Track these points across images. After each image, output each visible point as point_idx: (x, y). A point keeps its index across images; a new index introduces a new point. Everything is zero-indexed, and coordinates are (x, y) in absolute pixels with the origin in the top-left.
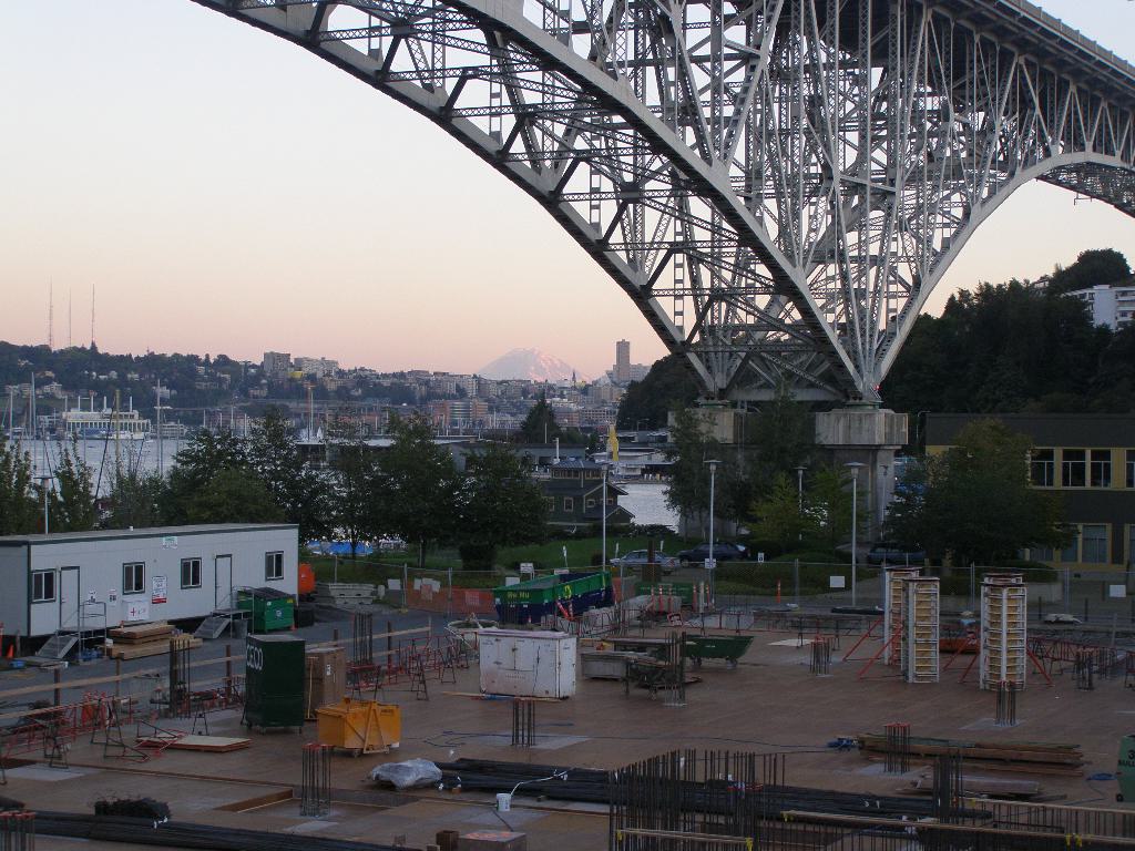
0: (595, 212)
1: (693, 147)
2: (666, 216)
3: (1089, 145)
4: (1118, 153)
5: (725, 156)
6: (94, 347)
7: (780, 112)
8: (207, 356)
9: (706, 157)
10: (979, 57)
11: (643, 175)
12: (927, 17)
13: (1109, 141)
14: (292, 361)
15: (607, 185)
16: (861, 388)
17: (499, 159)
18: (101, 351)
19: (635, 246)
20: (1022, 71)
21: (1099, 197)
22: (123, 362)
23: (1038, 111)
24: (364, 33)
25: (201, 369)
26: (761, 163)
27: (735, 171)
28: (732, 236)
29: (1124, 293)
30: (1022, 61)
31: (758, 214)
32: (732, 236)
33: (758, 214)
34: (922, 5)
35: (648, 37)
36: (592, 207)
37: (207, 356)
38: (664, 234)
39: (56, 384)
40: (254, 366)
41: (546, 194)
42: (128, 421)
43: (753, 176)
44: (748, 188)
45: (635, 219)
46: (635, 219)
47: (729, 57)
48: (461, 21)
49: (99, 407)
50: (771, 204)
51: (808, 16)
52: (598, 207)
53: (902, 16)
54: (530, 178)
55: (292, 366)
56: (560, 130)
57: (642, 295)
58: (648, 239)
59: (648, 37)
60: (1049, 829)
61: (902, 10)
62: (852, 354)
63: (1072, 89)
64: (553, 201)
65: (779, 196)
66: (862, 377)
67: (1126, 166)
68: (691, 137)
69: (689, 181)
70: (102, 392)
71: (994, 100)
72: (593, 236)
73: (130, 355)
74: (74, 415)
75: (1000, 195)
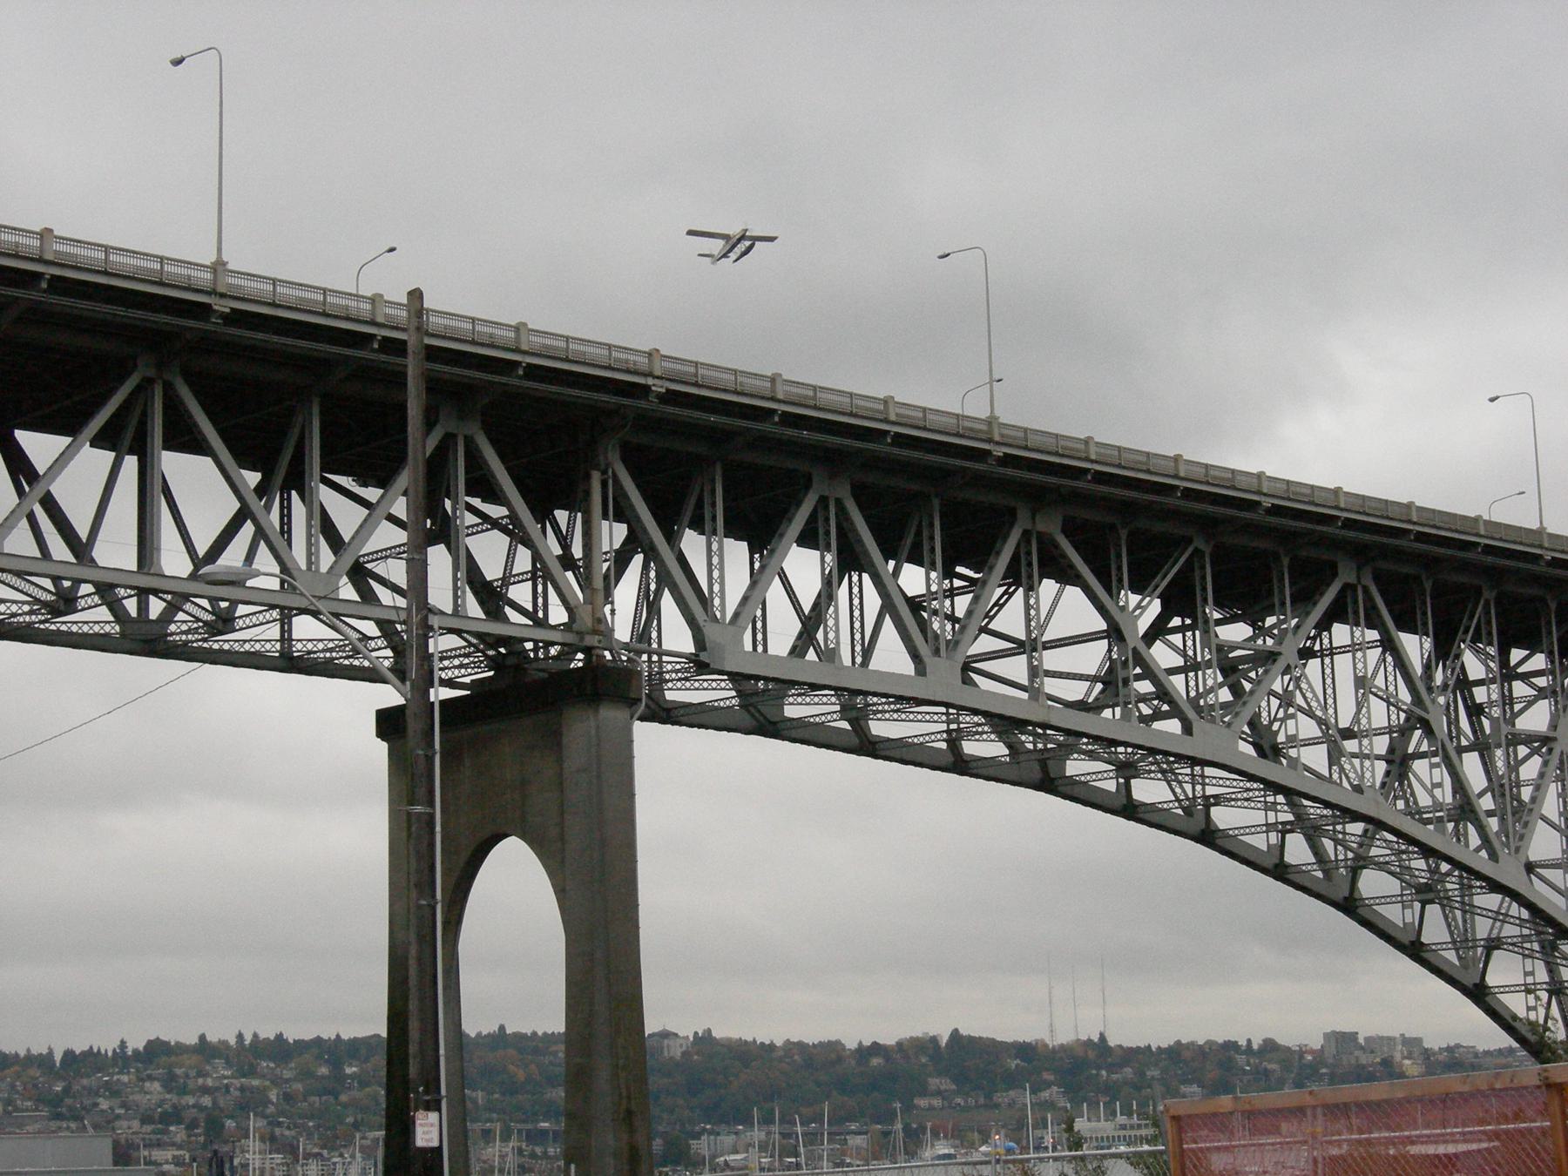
1: (1478, 850)
6: (1102, 1037)
8: (1249, 1041)
9: (1493, 856)
14: (1361, 1041)
17: (1280, 871)
18: (1112, 1043)
24: (1111, 774)
25: (1241, 1059)
37: (1249, 1041)
39: (1055, 1088)
40: (1312, 1052)
41: (1341, 902)
55: (1362, 1048)
57: (1479, 994)
60: (154, 1142)
68: (1474, 840)
73: (1149, 1046)
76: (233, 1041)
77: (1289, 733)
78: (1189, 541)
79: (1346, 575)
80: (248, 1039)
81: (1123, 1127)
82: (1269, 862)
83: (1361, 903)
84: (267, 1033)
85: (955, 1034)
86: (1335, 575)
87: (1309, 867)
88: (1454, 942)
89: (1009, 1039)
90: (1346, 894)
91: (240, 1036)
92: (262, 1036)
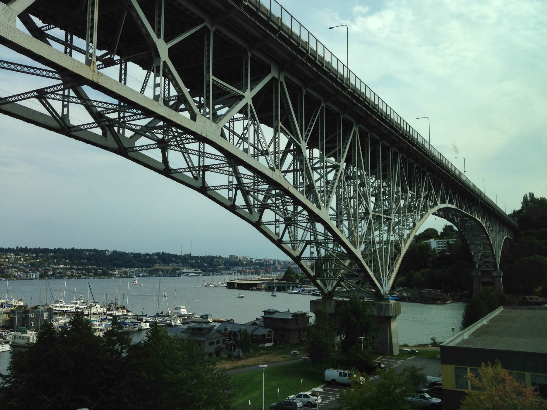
0: (277, 229)
2: (306, 231)
3: (447, 201)
4: (455, 204)
5: (327, 206)
7: (348, 189)
10: (416, 172)
11: (296, 213)
12: (399, 157)
13: (452, 200)
15: (281, 219)
16: (382, 292)
17: (233, 208)
19: (294, 242)
20: (428, 178)
21: (443, 218)
22: (197, 258)
23: (433, 191)
26: (342, 208)
27: (331, 212)
28: (331, 238)
29: (439, 242)
30: (428, 174)
31: (341, 229)
32: (331, 238)
33: (341, 229)
34: (398, 153)
35: (298, 163)
36: (276, 227)
38: (306, 236)
42: (197, 272)
43: (339, 213)
44: (337, 218)
45: (294, 234)
46: (294, 234)
47: (329, 167)
48: (192, 139)
49: (191, 269)
50: (346, 223)
51: (359, 153)
52: (278, 227)
53: (391, 156)
54: (248, 217)
56: (261, 197)
58: (299, 239)
59: (298, 163)
61: (391, 153)
62: (378, 278)
63: (442, 184)
64: (258, 225)
65: (349, 220)
66: (383, 288)
67: (457, 208)
69: (314, 218)
70: (192, 265)
71: (421, 186)
72: (276, 238)
74: (185, 270)
75: (424, 218)
76: (15, 249)
77: (230, 196)
78: (204, 22)
79: (274, 74)
80: (19, 248)
81: (193, 271)
82: (229, 204)
83: (263, 224)
84: (24, 247)
85: (163, 252)
86: (269, 72)
87: (243, 207)
88: (291, 241)
89: (173, 254)
90: (257, 220)
91: (17, 247)
92: (23, 247)
